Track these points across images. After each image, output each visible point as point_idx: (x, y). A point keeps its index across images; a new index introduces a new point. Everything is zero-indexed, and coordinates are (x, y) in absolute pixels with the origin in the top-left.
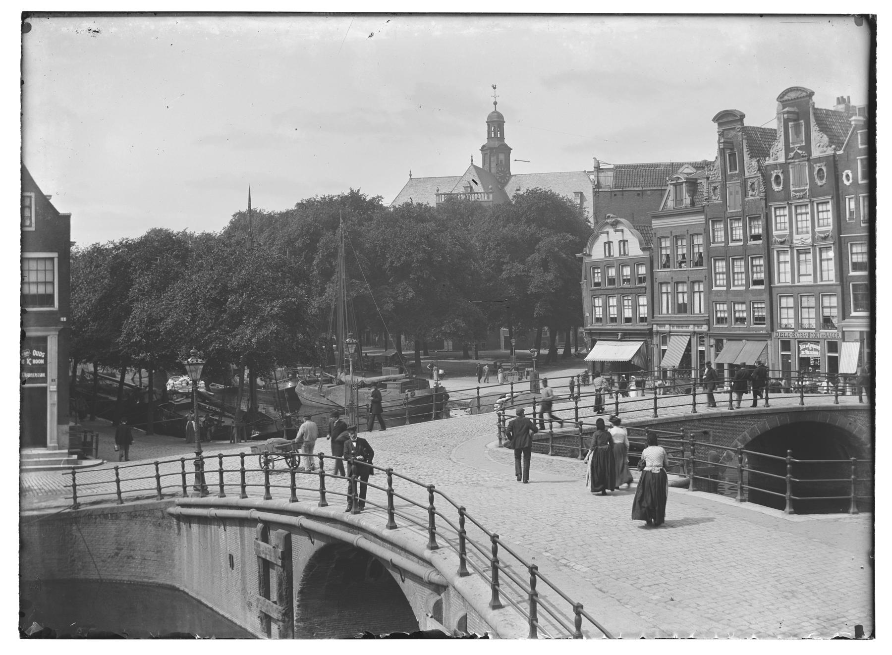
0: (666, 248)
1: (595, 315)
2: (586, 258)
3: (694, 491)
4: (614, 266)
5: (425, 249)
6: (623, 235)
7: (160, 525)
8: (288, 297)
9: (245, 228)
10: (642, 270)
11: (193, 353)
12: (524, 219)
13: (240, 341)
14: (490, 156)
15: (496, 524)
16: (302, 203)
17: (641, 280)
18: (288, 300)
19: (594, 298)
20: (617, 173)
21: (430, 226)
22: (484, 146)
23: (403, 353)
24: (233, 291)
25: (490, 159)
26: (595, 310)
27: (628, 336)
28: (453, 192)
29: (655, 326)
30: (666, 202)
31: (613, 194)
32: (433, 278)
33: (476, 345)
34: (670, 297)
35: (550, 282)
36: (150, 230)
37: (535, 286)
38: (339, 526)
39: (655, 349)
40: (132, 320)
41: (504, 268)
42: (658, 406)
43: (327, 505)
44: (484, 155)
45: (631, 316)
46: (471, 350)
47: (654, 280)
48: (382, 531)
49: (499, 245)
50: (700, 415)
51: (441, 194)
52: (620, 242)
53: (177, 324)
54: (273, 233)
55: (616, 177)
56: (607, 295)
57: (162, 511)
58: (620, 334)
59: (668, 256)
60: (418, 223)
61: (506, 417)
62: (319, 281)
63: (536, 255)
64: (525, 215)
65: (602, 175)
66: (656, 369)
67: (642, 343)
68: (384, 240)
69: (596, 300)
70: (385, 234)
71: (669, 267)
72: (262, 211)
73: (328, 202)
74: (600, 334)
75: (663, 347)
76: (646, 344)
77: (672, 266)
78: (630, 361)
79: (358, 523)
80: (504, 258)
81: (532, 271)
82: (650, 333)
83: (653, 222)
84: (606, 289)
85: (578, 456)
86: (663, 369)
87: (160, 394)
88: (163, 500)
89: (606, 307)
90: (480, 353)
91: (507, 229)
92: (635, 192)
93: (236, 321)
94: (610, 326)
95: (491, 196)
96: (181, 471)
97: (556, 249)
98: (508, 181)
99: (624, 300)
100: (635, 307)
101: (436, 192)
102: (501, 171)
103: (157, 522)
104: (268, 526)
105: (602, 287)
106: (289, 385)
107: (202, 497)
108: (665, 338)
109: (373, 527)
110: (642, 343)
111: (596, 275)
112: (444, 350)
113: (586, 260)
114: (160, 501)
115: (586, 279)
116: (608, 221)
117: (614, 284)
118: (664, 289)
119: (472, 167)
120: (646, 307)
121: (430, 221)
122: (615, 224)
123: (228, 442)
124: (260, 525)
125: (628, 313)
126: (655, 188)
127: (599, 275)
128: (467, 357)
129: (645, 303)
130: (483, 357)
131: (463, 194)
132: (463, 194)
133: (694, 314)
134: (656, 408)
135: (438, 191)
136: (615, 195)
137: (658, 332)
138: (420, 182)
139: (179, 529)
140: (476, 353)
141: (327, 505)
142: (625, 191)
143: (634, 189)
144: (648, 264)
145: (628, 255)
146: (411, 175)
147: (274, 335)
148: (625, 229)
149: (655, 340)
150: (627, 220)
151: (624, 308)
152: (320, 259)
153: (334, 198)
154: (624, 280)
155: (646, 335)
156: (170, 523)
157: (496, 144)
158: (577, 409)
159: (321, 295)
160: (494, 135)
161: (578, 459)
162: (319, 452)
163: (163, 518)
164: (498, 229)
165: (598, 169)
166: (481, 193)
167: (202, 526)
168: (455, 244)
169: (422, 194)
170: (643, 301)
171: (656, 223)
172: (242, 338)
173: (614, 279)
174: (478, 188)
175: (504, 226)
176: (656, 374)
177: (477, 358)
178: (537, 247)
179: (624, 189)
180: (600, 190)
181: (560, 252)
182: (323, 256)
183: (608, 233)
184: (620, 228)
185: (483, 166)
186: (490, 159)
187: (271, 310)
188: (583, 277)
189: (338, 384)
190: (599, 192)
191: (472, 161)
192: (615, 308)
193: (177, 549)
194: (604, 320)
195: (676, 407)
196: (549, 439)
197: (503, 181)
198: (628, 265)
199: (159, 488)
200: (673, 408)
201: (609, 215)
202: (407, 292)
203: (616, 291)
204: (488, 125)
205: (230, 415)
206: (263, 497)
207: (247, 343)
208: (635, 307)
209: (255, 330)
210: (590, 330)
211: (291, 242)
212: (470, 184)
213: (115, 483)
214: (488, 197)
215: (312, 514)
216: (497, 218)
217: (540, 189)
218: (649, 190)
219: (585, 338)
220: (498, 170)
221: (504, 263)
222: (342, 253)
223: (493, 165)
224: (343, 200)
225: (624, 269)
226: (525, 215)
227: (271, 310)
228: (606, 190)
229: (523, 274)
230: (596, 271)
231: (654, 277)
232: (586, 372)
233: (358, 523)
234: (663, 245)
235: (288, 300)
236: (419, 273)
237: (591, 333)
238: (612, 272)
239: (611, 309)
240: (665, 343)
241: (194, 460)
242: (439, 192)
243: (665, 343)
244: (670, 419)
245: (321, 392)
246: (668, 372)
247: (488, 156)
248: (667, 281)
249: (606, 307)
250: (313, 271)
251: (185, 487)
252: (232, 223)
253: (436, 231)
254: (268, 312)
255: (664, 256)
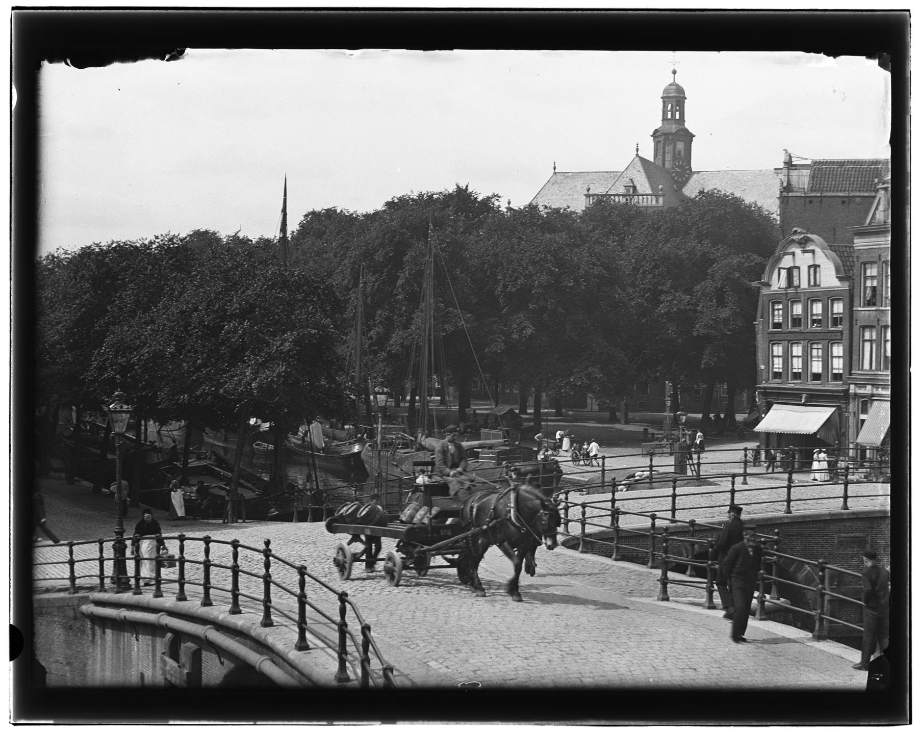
0: (872, 278)
1: (773, 368)
2: (764, 288)
3: (761, 620)
4: (800, 301)
5: (550, 269)
6: (814, 258)
7: (70, 628)
8: (307, 327)
9: (320, 234)
10: (838, 308)
11: (117, 396)
12: (694, 232)
13: (236, 385)
14: (664, 144)
15: (448, 651)
16: (393, 202)
17: (836, 322)
18: (305, 331)
19: (773, 344)
20: (815, 170)
21: (561, 237)
22: (656, 131)
23: (542, 411)
24: (233, 316)
25: (664, 148)
26: (773, 361)
27: (815, 399)
28: (609, 193)
29: (852, 387)
30: (874, 214)
31: (808, 200)
32: (560, 310)
33: (626, 405)
34: (874, 346)
35: (726, 321)
36: (192, 233)
37: (704, 325)
38: (248, 642)
39: (852, 420)
40: (105, 350)
41: (662, 298)
42: (792, 498)
43: (240, 612)
44: (657, 144)
45: (820, 371)
46: (619, 410)
47: (854, 322)
48: (288, 653)
49: (656, 267)
50: (853, 513)
51: (593, 195)
52: (810, 267)
53: (157, 356)
54: (347, 241)
55: (813, 177)
56: (789, 341)
57: (74, 609)
58: (804, 396)
59: (874, 289)
60: (543, 233)
61: (570, 505)
62: (404, 308)
63: (708, 283)
64: (694, 228)
65: (794, 173)
66: (851, 446)
67: (834, 409)
68: (496, 255)
69: (775, 348)
70: (497, 247)
71: (874, 304)
72: (345, 211)
73: (426, 202)
74: (779, 394)
75: (862, 417)
76: (840, 412)
77: (878, 303)
78: (815, 434)
79: (265, 639)
80: (663, 284)
81: (701, 304)
82: (846, 396)
83: (856, 241)
84: (790, 333)
85: (648, 563)
86: (861, 446)
87: (168, 453)
88: (76, 595)
89: (787, 357)
90: (631, 415)
91: (669, 245)
92: (838, 199)
93: (237, 356)
94: (791, 385)
95: (661, 200)
96: (98, 555)
97: (737, 275)
98: (688, 180)
99: (812, 349)
100: (826, 360)
101: (586, 193)
102: (679, 167)
103: (67, 623)
104: (179, 636)
105: (784, 329)
106: (356, 448)
107: (117, 593)
108: (866, 403)
109: (280, 646)
110: (834, 409)
111: (776, 313)
112: (586, 410)
113: (764, 291)
114: (72, 596)
115: (762, 318)
116: (795, 237)
117: (800, 326)
118: (867, 336)
119: (637, 159)
120: (841, 360)
121: (561, 232)
122: (804, 243)
123: (221, 521)
124: (169, 635)
125: (817, 367)
126: (866, 194)
127: (781, 312)
128: (614, 420)
129: (841, 354)
130: (635, 421)
131: (623, 196)
132: (623, 196)
133: (862, 370)
134: (789, 501)
135: (588, 190)
136: (811, 202)
137: (856, 394)
138: (567, 177)
139: (94, 635)
140: (626, 415)
141: (240, 612)
142: (824, 196)
143: (837, 194)
144: (847, 300)
145: (819, 286)
146: (555, 168)
147: (282, 379)
148: (818, 251)
149: (852, 406)
150: (824, 238)
151: (811, 361)
152: (407, 278)
153: (435, 196)
154: (814, 321)
155: (839, 399)
156: (84, 626)
157: (674, 128)
158: (674, 496)
159: (406, 327)
160: (672, 116)
161: (648, 567)
162: (233, 539)
163: (75, 618)
164: (657, 244)
165: (789, 165)
166: (647, 195)
167: (115, 632)
168: (594, 264)
169: (569, 195)
170: (838, 350)
171: (860, 243)
172: (241, 380)
173: (800, 319)
174: (644, 186)
175: (667, 241)
176: (851, 453)
177: (627, 423)
178: (710, 271)
179: (851, 195)
180: (790, 194)
181: (742, 279)
182: (409, 274)
183: (793, 254)
184: (811, 248)
185: (654, 159)
186: (664, 148)
187: (281, 345)
188: (759, 315)
189: (418, 450)
190: (788, 197)
191: (637, 150)
192: (800, 359)
193: (90, 662)
194: (784, 376)
195: (825, 501)
196: (613, 538)
197: (680, 179)
198: (819, 300)
199: (73, 578)
200: (820, 501)
201: (795, 229)
202: (525, 328)
203: (803, 336)
204: (664, 102)
205: (250, 485)
206: (176, 595)
207: (246, 388)
208: (826, 360)
209: (257, 372)
210: (765, 388)
211: (368, 254)
212: (633, 183)
213: (67, 565)
214: (657, 201)
215: (220, 623)
216: (658, 229)
217: (719, 191)
218: (858, 196)
219: (757, 400)
220: (675, 164)
221: (662, 292)
222: (430, 271)
223: (668, 157)
224: (448, 199)
225: (814, 306)
226: (694, 228)
227: (281, 345)
228: (799, 194)
229: (688, 308)
230: (776, 308)
231: (854, 319)
232: (758, 446)
233: (265, 639)
234: (868, 273)
235: (305, 331)
236: (542, 303)
237: (766, 393)
238: (798, 309)
239: (795, 360)
240: (865, 411)
241: (113, 543)
242: (591, 192)
243: (865, 411)
244: (809, 516)
245: (394, 460)
246: (868, 451)
247: (661, 144)
248: (871, 324)
249: (787, 357)
250: (397, 295)
251: (102, 576)
252: (302, 226)
253: (568, 245)
254: (277, 347)
255: (868, 289)
